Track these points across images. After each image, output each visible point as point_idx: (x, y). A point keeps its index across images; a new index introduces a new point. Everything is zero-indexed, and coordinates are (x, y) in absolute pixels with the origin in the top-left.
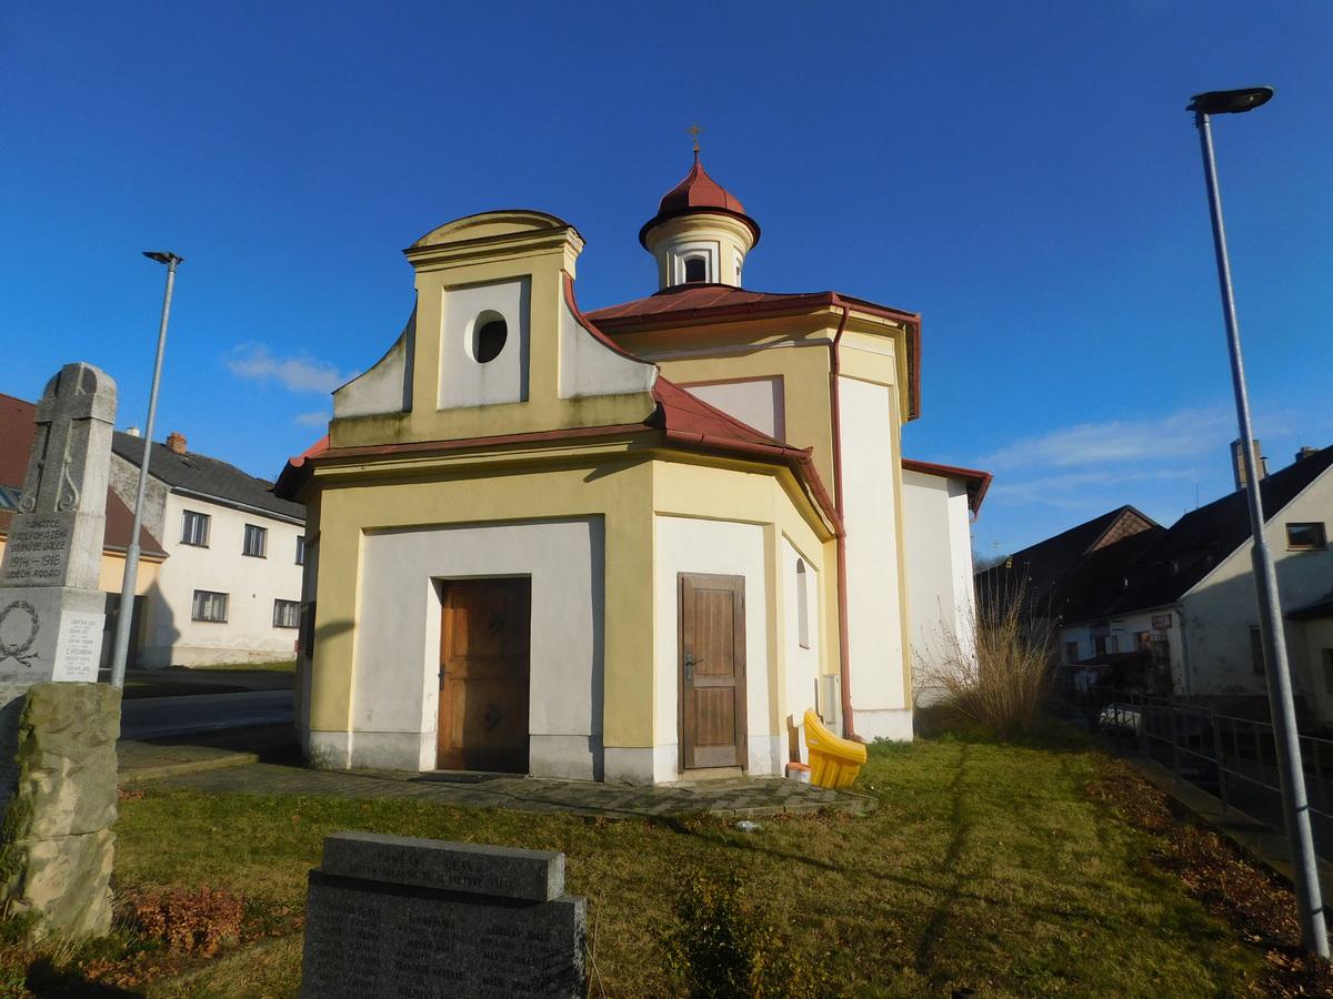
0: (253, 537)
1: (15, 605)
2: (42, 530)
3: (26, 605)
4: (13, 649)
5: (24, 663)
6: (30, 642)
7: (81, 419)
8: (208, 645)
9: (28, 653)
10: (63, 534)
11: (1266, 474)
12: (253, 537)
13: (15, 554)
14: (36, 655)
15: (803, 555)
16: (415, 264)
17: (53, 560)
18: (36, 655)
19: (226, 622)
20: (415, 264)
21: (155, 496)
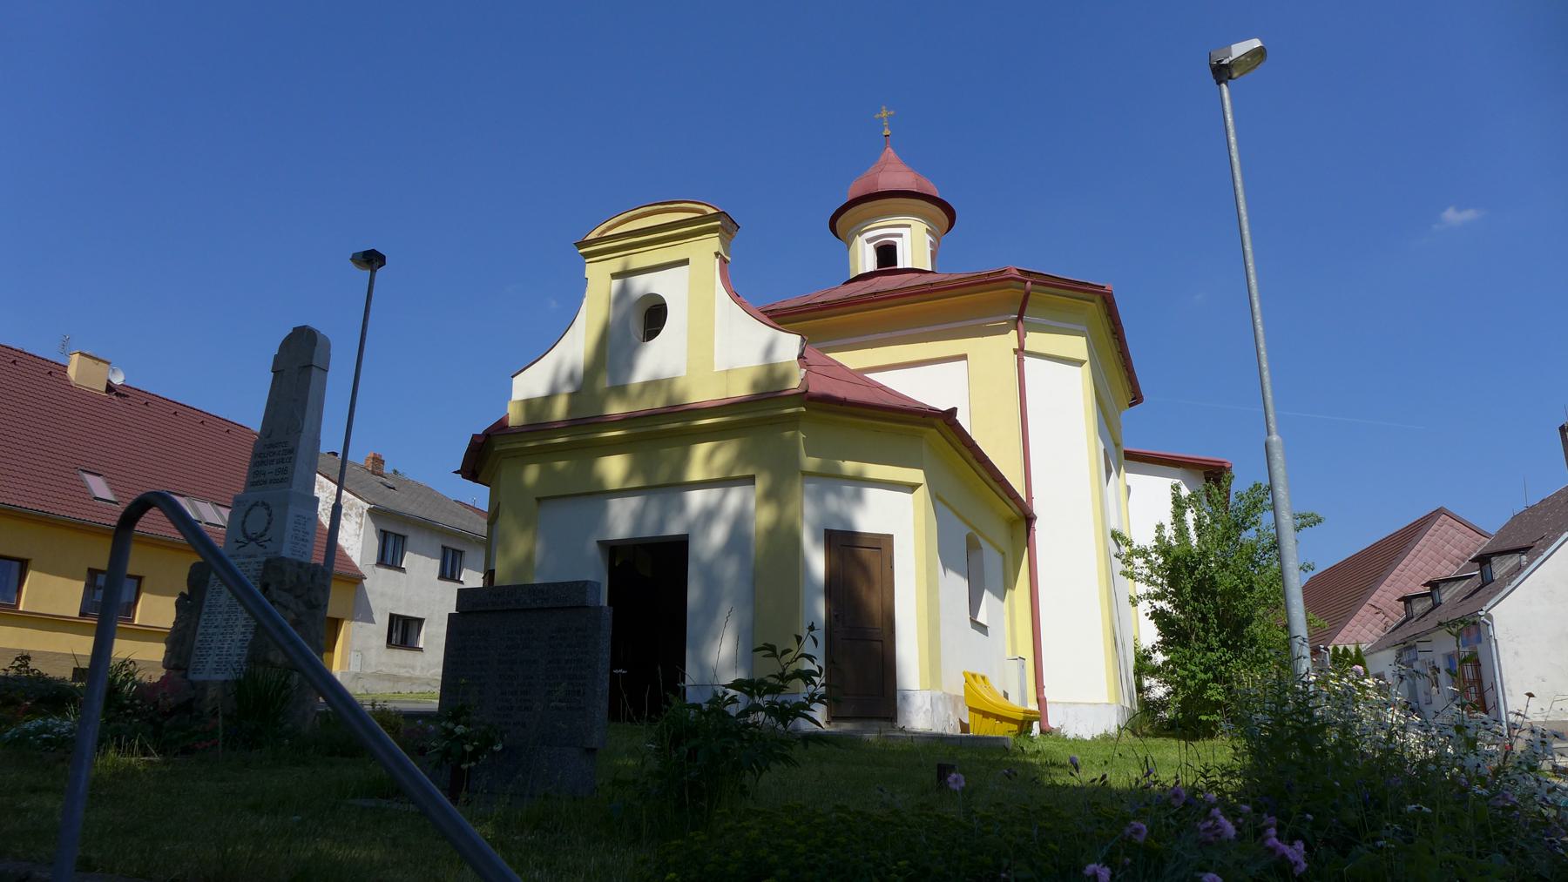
0: (449, 572)
1: (256, 504)
2: (275, 449)
3: (263, 504)
4: (254, 536)
5: (262, 546)
6: (266, 530)
7: (305, 367)
8: (402, 672)
9: (264, 538)
10: (291, 451)
11: (373, 272)
12: (449, 572)
13: (256, 469)
14: (270, 540)
15: (975, 529)
16: (587, 255)
17: (284, 471)
18: (270, 540)
19: (403, 570)
20: (587, 255)
21: (353, 515)
